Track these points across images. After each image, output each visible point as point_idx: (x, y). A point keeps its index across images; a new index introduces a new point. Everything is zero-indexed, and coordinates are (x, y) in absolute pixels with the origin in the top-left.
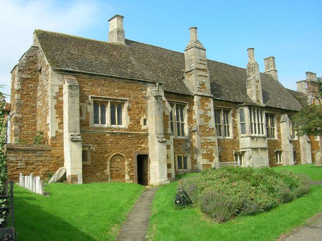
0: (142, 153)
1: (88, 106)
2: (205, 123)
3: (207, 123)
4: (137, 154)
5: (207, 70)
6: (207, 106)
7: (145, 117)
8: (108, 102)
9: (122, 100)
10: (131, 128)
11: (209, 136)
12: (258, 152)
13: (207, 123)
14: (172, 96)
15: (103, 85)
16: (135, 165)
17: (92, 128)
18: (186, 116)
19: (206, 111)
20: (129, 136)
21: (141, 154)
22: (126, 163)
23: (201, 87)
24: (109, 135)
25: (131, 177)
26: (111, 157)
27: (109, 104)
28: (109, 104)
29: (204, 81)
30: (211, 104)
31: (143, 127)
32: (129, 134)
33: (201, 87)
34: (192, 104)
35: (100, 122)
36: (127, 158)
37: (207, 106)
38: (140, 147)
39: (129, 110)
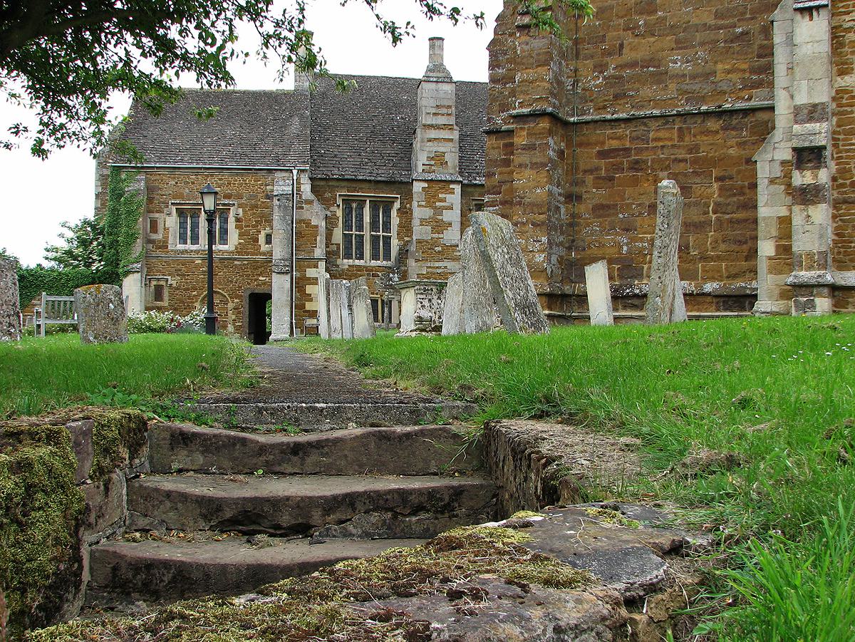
0: (259, 290)
1: (167, 218)
2: (434, 235)
3: (441, 236)
4: (249, 292)
5: (455, 127)
6: (443, 200)
7: (268, 230)
8: (366, 201)
9: (224, 205)
10: (240, 250)
11: (441, 260)
12: (811, 19)
13: (441, 236)
14: (363, 186)
15: (193, 183)
16: (245, 310)
17: (172, 251)
18: (395, 220)
19: (439, 211)
20: (236, 262)
21: (256, 291)
22: (230, 305)
23: (433, 163)
24: (200, 261)
25: (237, 329)
26: (202, 296)
27: (368, 202)
28: (368, 202)
29: (442, 149)
30: (454, 197)
31: (265, 248)
32: (235, 259)
33: (433, 163)
34: (408, 195)
35: (189, 241)
36: (231, 298)
37: (443, 200)
38: (255, 280)
39: (238, 220)
